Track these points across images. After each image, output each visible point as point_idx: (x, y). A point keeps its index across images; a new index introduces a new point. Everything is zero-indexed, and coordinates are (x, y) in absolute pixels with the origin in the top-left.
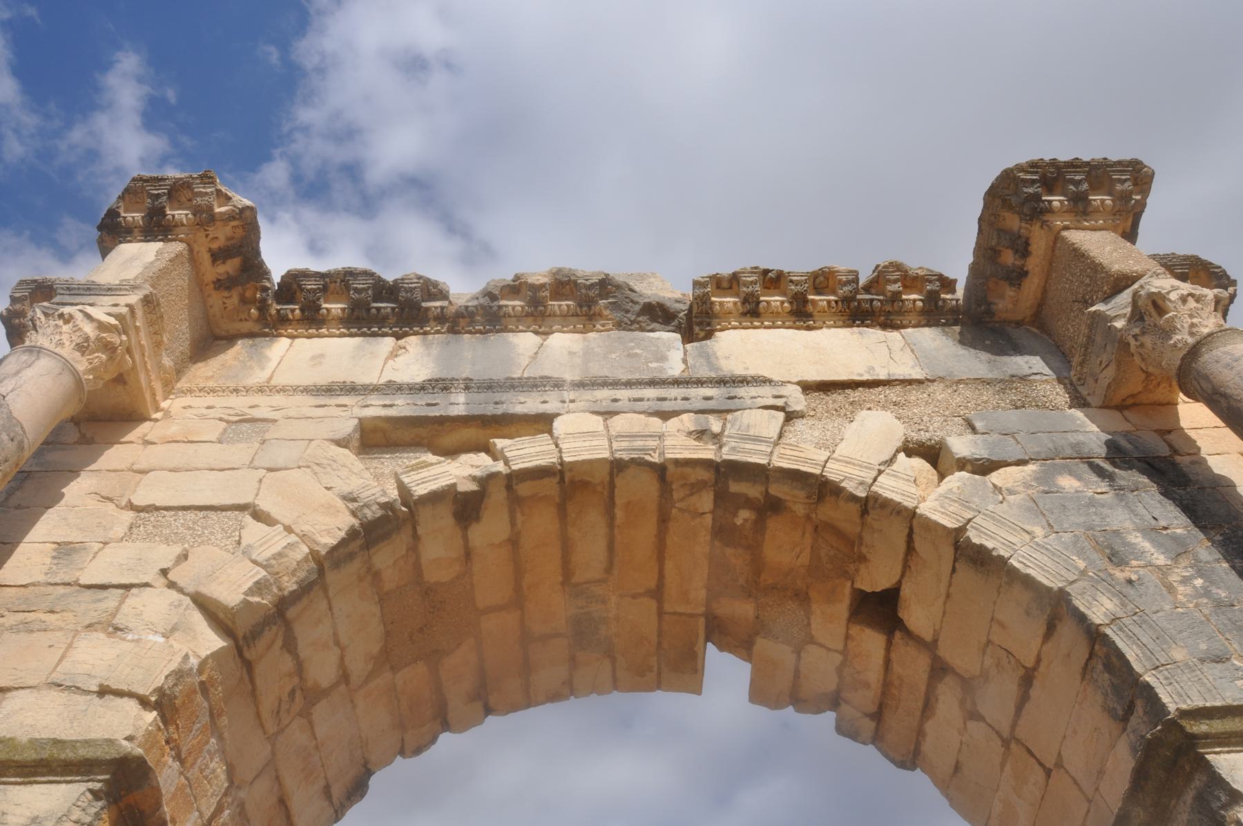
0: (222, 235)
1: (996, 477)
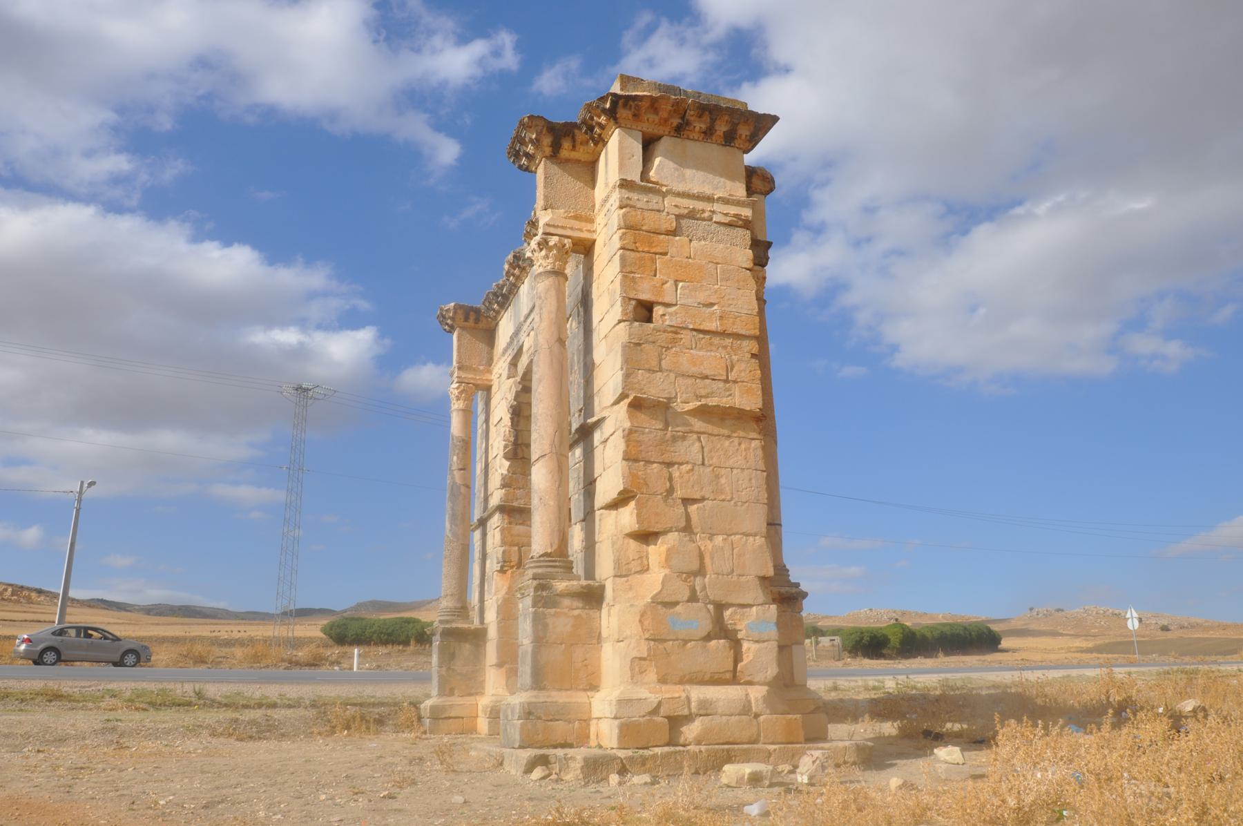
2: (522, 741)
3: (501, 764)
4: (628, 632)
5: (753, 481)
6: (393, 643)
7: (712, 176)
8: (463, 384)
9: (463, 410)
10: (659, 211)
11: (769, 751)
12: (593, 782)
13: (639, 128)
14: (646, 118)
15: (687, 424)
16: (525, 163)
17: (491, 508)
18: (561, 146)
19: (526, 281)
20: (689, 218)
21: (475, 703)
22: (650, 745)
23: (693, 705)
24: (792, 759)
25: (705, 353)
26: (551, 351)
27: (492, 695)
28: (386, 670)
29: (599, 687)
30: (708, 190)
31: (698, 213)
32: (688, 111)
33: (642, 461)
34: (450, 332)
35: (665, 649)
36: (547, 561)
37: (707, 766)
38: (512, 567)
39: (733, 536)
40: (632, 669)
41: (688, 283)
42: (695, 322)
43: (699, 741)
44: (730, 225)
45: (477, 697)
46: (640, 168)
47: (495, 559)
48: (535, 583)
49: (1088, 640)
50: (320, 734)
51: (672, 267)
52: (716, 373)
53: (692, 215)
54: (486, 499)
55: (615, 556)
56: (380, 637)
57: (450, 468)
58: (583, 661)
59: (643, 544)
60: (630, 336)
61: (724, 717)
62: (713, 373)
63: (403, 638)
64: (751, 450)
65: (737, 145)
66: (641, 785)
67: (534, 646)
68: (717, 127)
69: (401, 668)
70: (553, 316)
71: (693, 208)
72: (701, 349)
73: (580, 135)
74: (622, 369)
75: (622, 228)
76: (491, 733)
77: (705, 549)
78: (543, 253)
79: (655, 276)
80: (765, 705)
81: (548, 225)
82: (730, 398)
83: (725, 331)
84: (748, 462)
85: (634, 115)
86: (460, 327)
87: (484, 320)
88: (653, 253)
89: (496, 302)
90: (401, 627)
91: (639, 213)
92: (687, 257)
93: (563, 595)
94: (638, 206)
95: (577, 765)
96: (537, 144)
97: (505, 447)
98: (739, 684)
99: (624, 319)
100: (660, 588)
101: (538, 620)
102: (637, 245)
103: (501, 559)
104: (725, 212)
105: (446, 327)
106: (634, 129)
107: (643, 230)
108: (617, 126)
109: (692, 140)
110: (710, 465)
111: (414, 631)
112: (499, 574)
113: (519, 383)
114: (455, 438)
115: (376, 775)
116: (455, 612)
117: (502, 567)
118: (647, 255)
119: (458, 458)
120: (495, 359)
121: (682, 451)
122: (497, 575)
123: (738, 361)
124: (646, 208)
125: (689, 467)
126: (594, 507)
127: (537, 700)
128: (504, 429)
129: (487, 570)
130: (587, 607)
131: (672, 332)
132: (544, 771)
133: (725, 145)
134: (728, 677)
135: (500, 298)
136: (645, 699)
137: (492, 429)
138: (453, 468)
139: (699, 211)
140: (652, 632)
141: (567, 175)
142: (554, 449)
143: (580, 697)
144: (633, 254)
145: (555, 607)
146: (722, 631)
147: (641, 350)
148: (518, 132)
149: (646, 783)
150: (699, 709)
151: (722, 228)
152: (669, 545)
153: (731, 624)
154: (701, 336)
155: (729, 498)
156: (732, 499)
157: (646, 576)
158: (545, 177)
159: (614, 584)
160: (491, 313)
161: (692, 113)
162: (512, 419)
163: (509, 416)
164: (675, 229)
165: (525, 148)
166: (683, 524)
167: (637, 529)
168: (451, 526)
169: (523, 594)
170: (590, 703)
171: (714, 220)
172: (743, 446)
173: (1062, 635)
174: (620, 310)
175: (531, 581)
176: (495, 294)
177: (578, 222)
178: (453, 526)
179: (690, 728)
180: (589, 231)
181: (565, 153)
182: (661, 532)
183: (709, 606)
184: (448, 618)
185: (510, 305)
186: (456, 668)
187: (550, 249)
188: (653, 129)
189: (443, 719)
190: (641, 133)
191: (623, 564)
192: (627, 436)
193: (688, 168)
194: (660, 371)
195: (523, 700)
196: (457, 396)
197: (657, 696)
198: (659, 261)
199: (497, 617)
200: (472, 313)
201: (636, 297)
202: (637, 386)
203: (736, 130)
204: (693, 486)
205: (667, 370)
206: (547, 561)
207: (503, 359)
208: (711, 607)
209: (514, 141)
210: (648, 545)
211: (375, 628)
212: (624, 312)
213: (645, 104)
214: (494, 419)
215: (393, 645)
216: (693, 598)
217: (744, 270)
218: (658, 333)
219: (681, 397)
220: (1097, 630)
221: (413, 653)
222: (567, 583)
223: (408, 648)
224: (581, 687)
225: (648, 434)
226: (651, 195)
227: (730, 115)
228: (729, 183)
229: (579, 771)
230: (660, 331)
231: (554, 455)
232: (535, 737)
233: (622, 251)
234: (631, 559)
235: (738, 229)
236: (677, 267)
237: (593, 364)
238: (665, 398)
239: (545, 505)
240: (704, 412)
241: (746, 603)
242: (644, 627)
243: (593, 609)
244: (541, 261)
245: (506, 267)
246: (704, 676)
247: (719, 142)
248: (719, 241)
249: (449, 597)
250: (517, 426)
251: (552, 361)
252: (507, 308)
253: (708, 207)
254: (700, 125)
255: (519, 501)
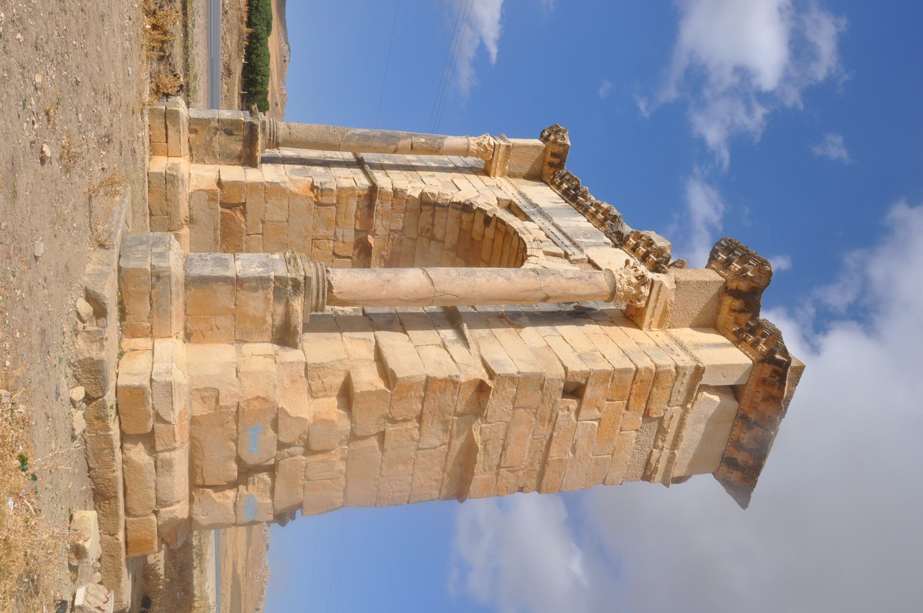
0: (557, 149)
2: (127, 270)
4: (246, 383)
6: (250, 12)
8: (492, 150)
10: (669, 402)
11: (116, 534)
13: (750, 382)
14: (760, 390)
15: (459, 433)
16: (720, 258)
18: (736, 298)
19: (590, 225)
20: (659, 428)
21: (182, 154)
22: (121, 416)
23: (167, 455)
26: (537, 290)
28: (223, 20)
30: (683, 444)
31: (662, 436)
32: (762, 430)
33: (425, 394)
34: (542, 136)
36: (324, 288)
37: (97, 478)
38: (316, 197)
39: (344, 478)
40: (206, 389)
41: (596, 430)
44: (648, 463)
45: (188, 156)
46: (712, 384)
48: (301, 279)
52: (507, 458)
53: (661, 431)
54: (382, 167)
55: (327, 363)
57: (414, 135)
58: (216, 326)
60: (550, 379)
61: (153, 484)
62: (508, 455)
63: (254, 20)
65: (721, 468)
67: (233, 278)
69: (225, 33)
70: (572, 292)
71: (667, 432)
72: (532, 443)
73: (744, 318)
74: (519, 373)
77: (332, 454)
78: (634, 280)
79: (607, 400)
81: (661, 285)
83: (548, 464)
84: (418, 488)
85: (764, 380)
86: (546, 148)
87: (551, 171)
88: (629, 398)
89: (569, 187)
91: (669, 385)
92: (621, 428)
93: (288, 305)
95: (94, 353)
96: (741, 276)
97: (433, 195)
98: (190, 490)
99: (568, 374)
100: (293, 416)
101: (262, 281)
103: (324, 187)
105: (546, 134)
106: (750, 377)
107: (652, 387)
109: (732, 428)
110: (417, 456)
111: (260, 31)
112: (310, 184)
113: (494, 215)
114: (443, 140)
115: (80, 115)
116: (273, 137)
117: (317, 187)
118: (628, 393)
121: (433, 430)
123: (518, 476)
124: (673, 391)
125: (417, 437)
126: (379, 329)
128: (450, 194)
129: (314, 168)
130: (274, 329)
132: (87, 315)
133: (722, 457)
134: (197, 481)
137: (447, 177)
138: (413, 138)
140: (247, 409)
141: (706, 302)
143: (177, 326)
144: (630, 379)
145: (274, 297)
146: (246, 472)
147: (535, 391)
149: (73, 430)
150: (162, 461)
153: (254, 480)
154: (545, 443)
155: (383, 473)
156: (382, 476)
157: (306, 396)
158: (707, 282)
159: (298, 363)
161: (760, 434)
162: (459, 203)
163: (463, 201)
165: (736, 261)
166: (358, 433)
167: (355, 391)
168: (357, 135)
169: (289, 263)
171: (654, 450)
172: (434, 483)
173: (248, 550)
174: (577, 370)
176: (577, 188)
177: (660, 312)
180: (651, 323)
181: (728, 301)
183: (273, 460)
184: (268, 130)
186: (217, 136)
187: (637, 287)
188: (749, 390)
189: (166, 122)
191: (319, 372)
192: (451, 380)
193: (707, 426)
196: (481, 143)
197: (177, 420)
198: (621, 403)
199: (267, 182)
200: (559, 160)
201: (589, 384)
203: (737, 470)
205: (514, 414)
206: (324, 288)
207: (515, 193)
208: (272, 462)
209: (744, 251)
210: (338, 396)
212: (575, 374)
214: (460, 179)
216: (281, 446)
217: (604, 478)
218: (551, 405)
219: (486, 427)
220: (250, 576)
223: (244, 25)
224: (189, 325)
225: (452, 398)
226: (685, 394)
229: (87, 356)
230: (553, 406)
231: (433, 295)
233: (635, 369)
234: (323, 380)
235: (643, 471)
236: (613, 420)
237: (521, 326)
240: (470, 450)
242: (251, 402)
243: (272, 335)
244: (626, 277)
245: (605, 205)
247: (727, 452)
248: (633, 455)
249: (288, 130)
250: (453, 208)
252: (563, 199)
253: (667, 445)
254: (746, 438)
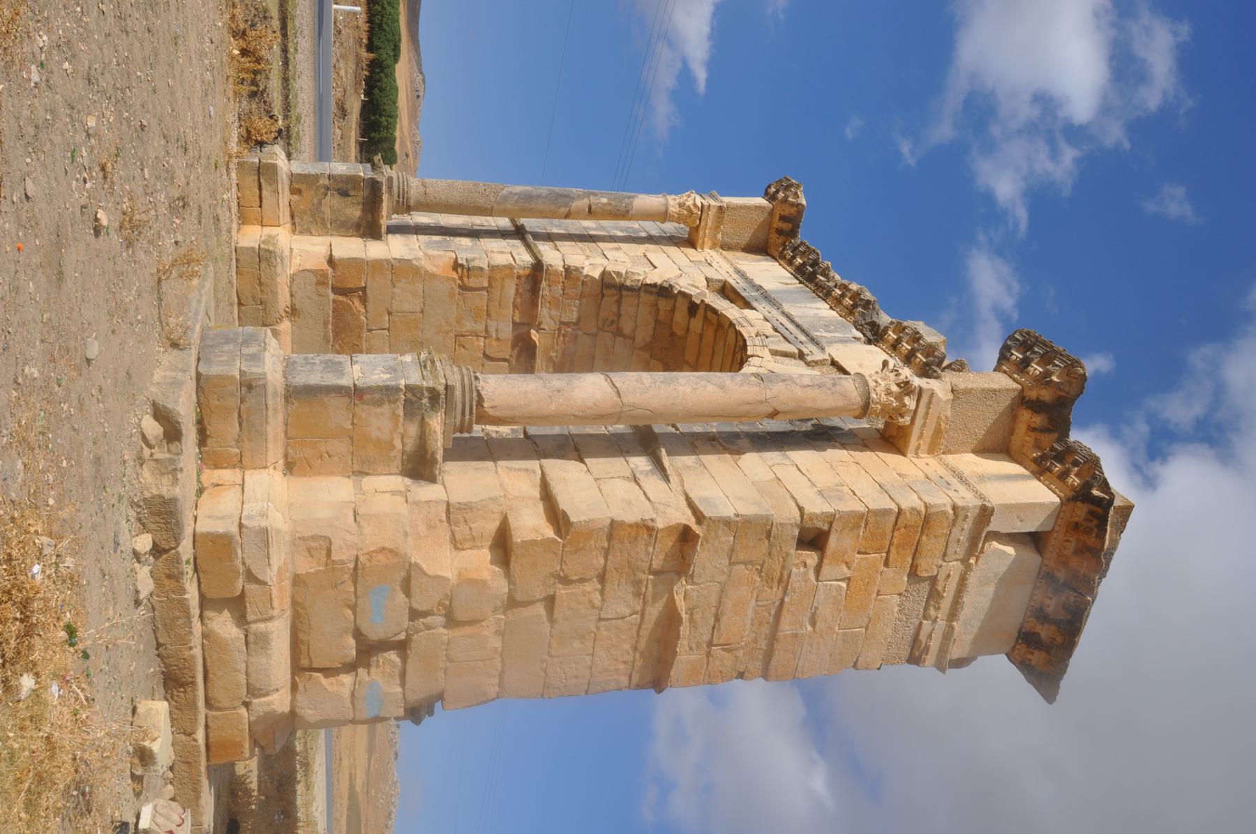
0: (788, 211)
1: (626, 619)
2: (208, 378)
3: (175, 345)
4: (368, 530)
5: (574, 681)
7: (983, 617)
8: (699, 213)
9: (667, 211)
10: (945, 555)
11: (194, 733)
12: (138, 513)
13: (1057, 528)
14: (1071, 539)
15: (656, 598)
16: (1014, 357)
17: (535, 245)
18: (1036, 412)
19: (834, 313)
20: (931, 591)
21: (281, 222)
22: (201, 575)
23: (262, 626)
24: (183, 763)
25: (749, 617)
26: (761, 402)
27: (291, 249)
29: (291, 473)
30: (965, 613)
35: (344, 582)
37: (168, 658)
38: (461, 278)
39: (499, 659)
40: (313, 538)
42: (792, 604)
43: (208, 636)
44: (916, 639)
45: (289, 225)
47: (473, 256)
48: (441, 389)
49: (363, 786)
50: (233, 17)
51: (868, 573)
53: (934, 595)
54: (549, 237)
55: (476, 503)
56: (377, 15)
57: (592, 194)
59: (493, 539)
60: (781, 524)
61: (244, 666)
62: (722, 628)
63: (377, 42)
64: (616, 677)
66: (134, 585)
67: (349, 388)
68: (1047, 626)
69: (338, 60)
71: (943, 597)
72: (756, 612)
73: (1048, 440)
74: (737, 515)
75: (926, 510)
76: (238, 251)
78: (895, 388)
79: (859, 553)
80: (262, 714)
81: (932, 395)
82: (687, 649)
83: (777, 640)
84: (600, 673)
86: (773, 209)
87: (780, 241)
90: (388, 41)
91: (945, 532)
93: (423, 424)
94: (954, 530)
95: (165, 488)
97: (618, 274)
98: (293, 675)
99: (805, 517)
100: (430, 573)
102: (903, 529)
103: (472, 264)
104: (933, 635)
105: (773, 190)
108: (1064, 500)
109: (1033, 592)
110: (598, 628)
112: (452, 261)
113: (702, 301)
115: (146, 171)
116: (403, 198)
117: (462, 266)
118: (887, 542)
119: (605, 204)
120: (729, 254)
121: (620, 594)
122: (450, 258)
123: (736, 657)
125: (598, 603)
126: (546, 457)
127: (270, 396)
128: (642, 273)
129: (458, 239)
130: (405, 457)
131: (782, 575)
132: (156, 437)
134: (302, 662)
135: (811, 270)
136: (269, 564)
138: (591, 198)
139: (939, 603)
140: (368, 565)
141: (995, 417)
142: (628, 409)
143: (275, 452)
145: (405, 414)
146: (368, 650)
147: (760, 540)
148: (1062, 355)
149: (137, 592)
150: (255, 634)
151: (912, 631)
152: (490, 582)
153: (378, 661)
154: (773, 612)
155: (553, 652)
156: (551, 656)
157: (448, 546)
158: (995, 390)
159: (437, 502)
160: (789, 252)
162: (655, 285)
163: (659, 282)
164: (917, 575)
166: (519, 597)
167: (514, 540)
168: (516, 194)
169: (425, 367)
170: (266, 467)
171: (924, 622)
172: (621, 666)
173: (369, 759)
175: (444, 381)
176: (815, 263)
177: (931, 433)
178: (516, 197)
179: (227, 623)
180: (918, 447)
181: (1025, 416)
182: (509, 571)
183: (404, 633)
184: (395, 189)
185: (801, 283)
186: (328, 198)
187: (899, 398)
189: (259, 179)
190: (1050, 529)
191: (465, 515)
192: (644, 525)
194: (730, 564)
195: (269, 377)
196: (684, 204)
198: (878, 557)
200: (790, 226)
201: (833, 530)
202: (713, 534)
203: (1040, 650)
204: (570, 608)
205: (730, 572)
207: (731, 270)
208: (402, 636)
209: (1047, 346)
210: (492, 548)
211: (389, 9)
212: (813, 517)
213: (1091, 540)
214: (656, 254)
215: (368, 31)
216: (414, 614)
217: (855, 660)
218: (781, 559)
219: (693, 590)
221: (358, 56)
222: (439, 433)
223: (364, 50)
224: (290, 451)
226: (967, 544)
227: (1063, 644)
228: (969, 638)
229: (155, 492)
230: (784, 561)
232: (215, 396)
234: (471, 526)
235: (909, 651)
237: (740, 452)
238: (693, 571)
239: (550, 397)
240: (670, 620)
241: (407, 679)
243: (403, 464)
244: (883, 383)
245: (854, 287)
246: (304, 632)
248: (895, 629)
250: (646, 292)
251: (749, 403)
252: (797, 278)
253: (942, 615)
255: (547, 289)
